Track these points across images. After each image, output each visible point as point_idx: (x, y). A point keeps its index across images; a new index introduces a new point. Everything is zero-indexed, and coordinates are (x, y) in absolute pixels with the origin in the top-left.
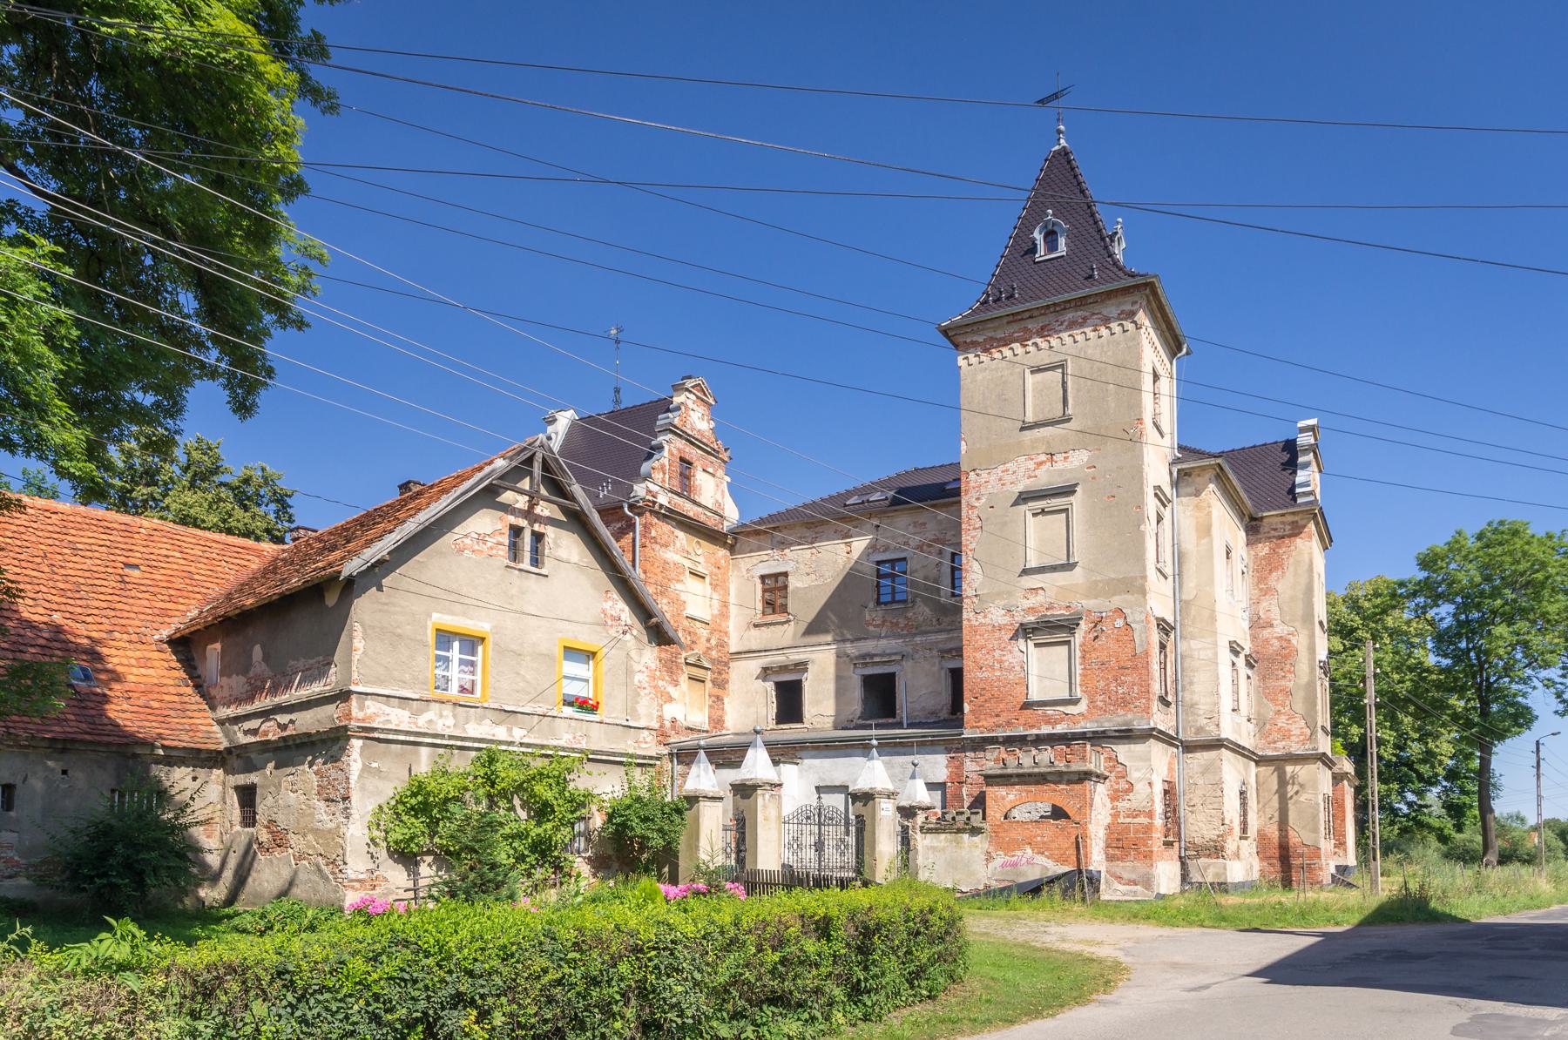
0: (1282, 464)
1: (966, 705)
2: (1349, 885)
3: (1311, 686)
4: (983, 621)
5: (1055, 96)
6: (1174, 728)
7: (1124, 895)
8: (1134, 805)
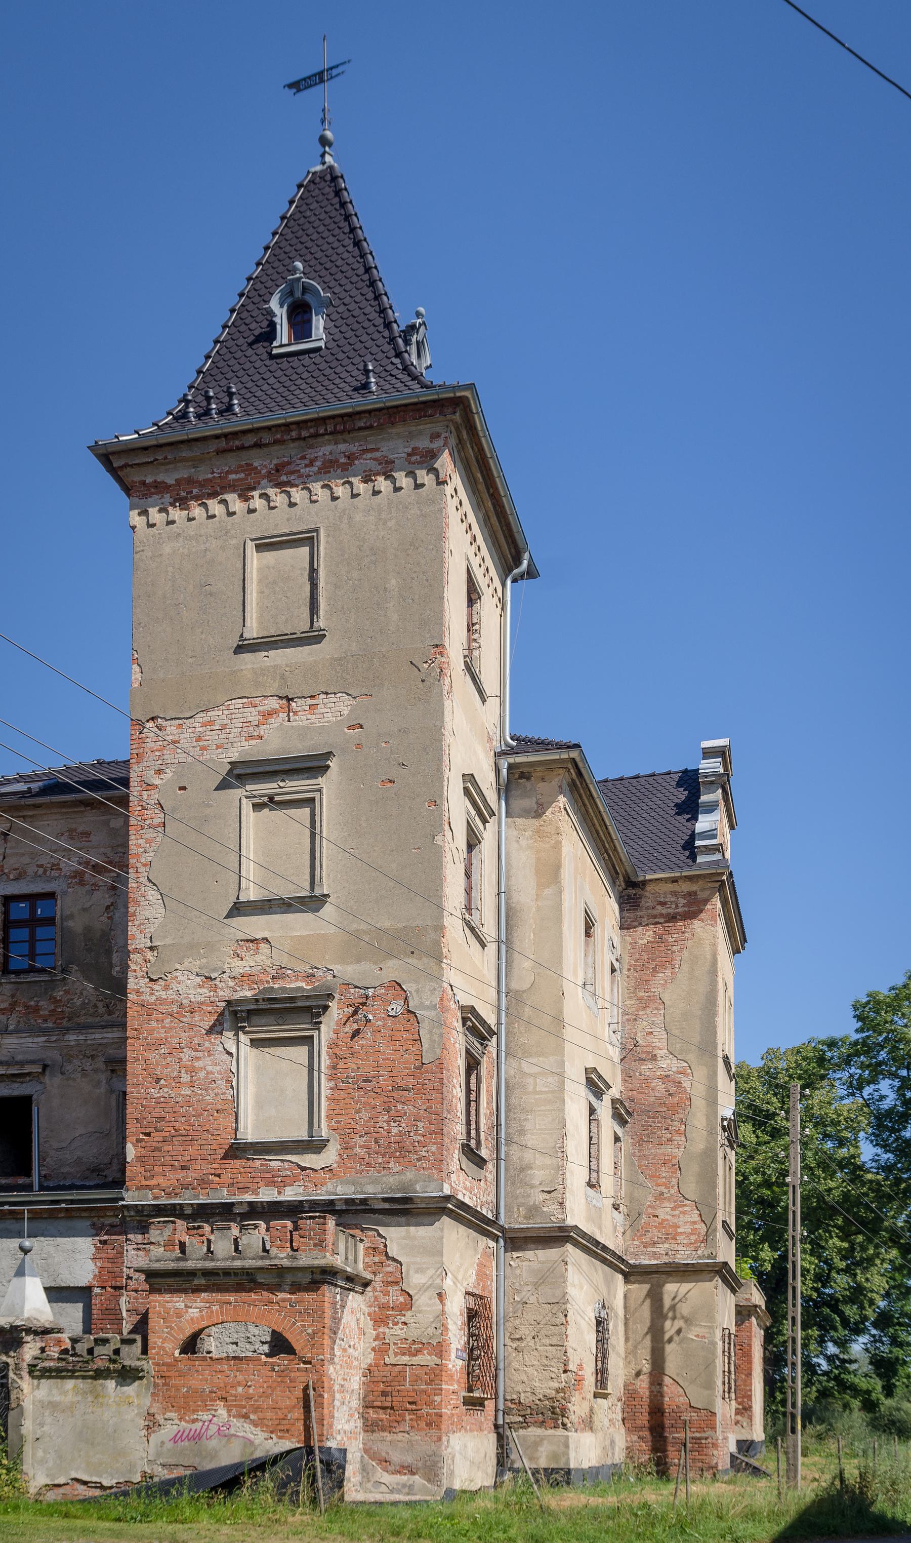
0: (676, 805)
1: (129, 1146)
2: (756, 1471)
3: (709, 1155)
4: (163, 994)
5: (318, 78)
6: (492, 1206)
7: (392, 1492)
8: (413, 1332)
